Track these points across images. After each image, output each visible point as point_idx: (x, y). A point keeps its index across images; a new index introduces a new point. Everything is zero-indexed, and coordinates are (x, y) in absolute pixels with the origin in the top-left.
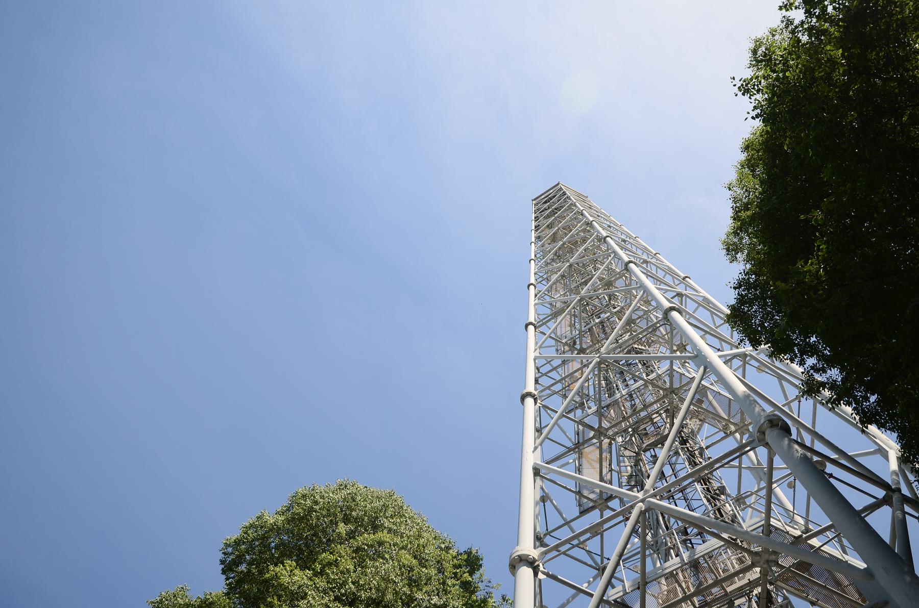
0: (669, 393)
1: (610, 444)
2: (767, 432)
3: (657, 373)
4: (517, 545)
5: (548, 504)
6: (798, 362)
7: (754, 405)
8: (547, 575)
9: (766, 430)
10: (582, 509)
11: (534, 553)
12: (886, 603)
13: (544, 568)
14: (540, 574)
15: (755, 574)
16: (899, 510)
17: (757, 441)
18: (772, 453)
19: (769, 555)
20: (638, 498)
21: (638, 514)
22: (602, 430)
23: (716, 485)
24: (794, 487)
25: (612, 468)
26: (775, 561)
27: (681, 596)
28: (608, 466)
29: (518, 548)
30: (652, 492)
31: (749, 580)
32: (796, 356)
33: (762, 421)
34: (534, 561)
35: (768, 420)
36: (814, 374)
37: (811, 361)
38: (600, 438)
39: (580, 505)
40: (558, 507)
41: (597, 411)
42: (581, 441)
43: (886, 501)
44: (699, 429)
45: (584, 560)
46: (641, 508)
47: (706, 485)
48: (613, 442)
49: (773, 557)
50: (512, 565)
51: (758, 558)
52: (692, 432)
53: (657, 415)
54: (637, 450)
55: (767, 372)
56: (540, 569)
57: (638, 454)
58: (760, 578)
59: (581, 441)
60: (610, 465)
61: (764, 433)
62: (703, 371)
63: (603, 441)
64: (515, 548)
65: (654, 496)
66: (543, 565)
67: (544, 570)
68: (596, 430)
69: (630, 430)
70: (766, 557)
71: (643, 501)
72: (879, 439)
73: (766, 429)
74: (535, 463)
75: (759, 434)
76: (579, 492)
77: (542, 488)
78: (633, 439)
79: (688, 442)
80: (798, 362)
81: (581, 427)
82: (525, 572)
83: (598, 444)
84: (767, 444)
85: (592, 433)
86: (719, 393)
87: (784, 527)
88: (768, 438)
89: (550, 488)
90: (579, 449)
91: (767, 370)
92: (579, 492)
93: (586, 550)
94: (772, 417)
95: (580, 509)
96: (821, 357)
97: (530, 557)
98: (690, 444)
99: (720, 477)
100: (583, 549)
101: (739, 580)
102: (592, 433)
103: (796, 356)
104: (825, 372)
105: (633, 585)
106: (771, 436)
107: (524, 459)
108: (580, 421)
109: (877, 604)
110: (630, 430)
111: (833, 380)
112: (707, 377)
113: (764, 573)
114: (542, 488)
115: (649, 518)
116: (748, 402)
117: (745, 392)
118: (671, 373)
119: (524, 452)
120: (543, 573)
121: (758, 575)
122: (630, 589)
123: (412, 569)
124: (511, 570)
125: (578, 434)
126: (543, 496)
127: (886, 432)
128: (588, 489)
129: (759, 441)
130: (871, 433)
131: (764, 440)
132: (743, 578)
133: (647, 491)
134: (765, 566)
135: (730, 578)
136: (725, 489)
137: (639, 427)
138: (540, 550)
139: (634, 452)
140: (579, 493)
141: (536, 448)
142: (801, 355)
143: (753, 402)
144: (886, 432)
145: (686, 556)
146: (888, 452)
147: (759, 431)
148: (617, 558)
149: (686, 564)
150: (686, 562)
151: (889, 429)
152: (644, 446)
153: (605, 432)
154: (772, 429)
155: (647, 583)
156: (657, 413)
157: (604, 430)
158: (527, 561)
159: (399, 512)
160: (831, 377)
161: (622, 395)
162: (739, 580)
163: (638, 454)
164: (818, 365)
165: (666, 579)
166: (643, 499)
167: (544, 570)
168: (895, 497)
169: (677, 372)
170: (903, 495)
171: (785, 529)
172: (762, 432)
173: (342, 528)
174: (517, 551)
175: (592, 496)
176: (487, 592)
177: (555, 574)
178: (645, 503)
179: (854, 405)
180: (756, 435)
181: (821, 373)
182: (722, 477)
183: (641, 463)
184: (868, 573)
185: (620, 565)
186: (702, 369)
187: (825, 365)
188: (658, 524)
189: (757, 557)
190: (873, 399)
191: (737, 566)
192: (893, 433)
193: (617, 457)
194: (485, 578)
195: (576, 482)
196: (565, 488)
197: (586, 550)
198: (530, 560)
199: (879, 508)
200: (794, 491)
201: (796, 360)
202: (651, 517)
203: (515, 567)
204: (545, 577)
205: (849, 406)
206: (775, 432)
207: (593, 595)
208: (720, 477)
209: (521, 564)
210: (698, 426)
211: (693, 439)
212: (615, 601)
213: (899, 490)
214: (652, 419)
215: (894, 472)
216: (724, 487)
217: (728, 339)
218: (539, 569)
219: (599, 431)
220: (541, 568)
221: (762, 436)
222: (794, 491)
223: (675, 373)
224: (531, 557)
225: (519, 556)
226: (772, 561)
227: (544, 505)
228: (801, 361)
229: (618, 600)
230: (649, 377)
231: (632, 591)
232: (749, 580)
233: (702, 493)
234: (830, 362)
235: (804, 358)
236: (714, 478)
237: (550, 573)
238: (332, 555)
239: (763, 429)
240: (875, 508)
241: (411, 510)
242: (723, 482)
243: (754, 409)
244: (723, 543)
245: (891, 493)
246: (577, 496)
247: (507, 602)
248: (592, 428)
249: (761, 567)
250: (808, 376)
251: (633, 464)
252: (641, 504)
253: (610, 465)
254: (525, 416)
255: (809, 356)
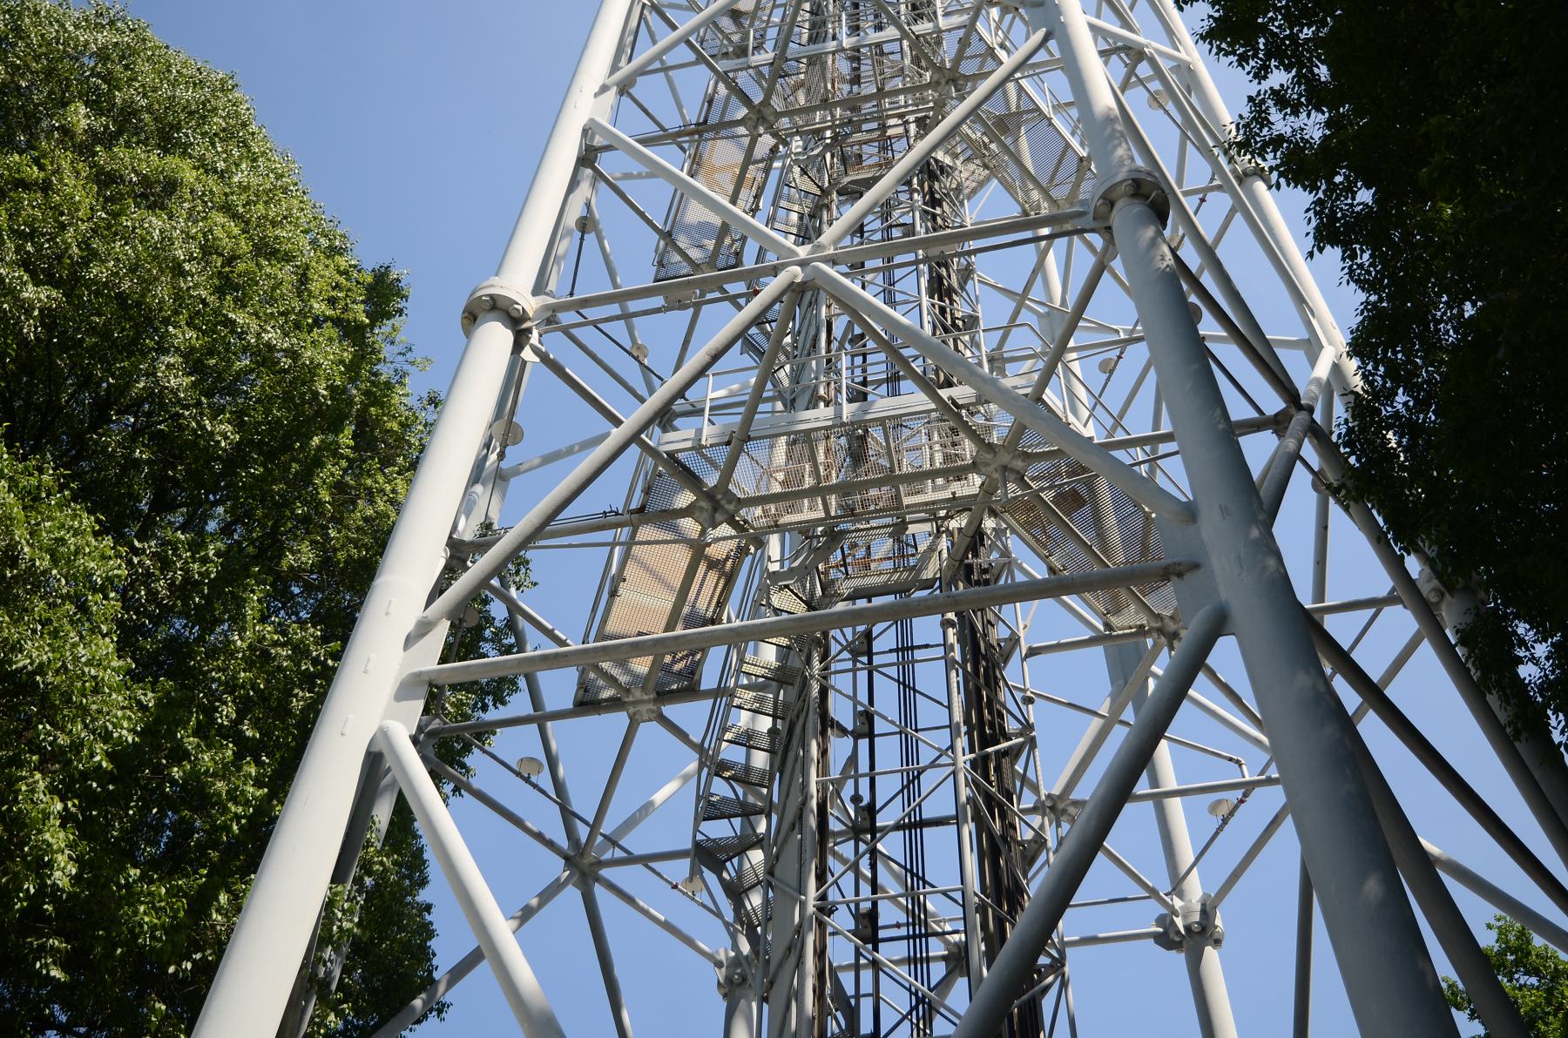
0: (943, 81)
1: (774, 150)
2: (1119, 205)
3: (937, 26)
4: (497, 275)
5: (590, 238)
6: (1253, 67)
7: (1116, 142)
8: (544, 358)
9: (1119, 198)
10: (662, 274)
11: (530, 304)
12: (1196, 566)
13: (540, 342)
14: (527, 350)
15: (973, 485)
16: (1295, 438)
17: (1091, 216)
18: (1109, 253)
19: (1014, 457)
20: (796, 254)
21: (785, 286)
22: (767, 112)
23: (961, 309)
24: (1111, 372)
25: (757, 206)
26: (1018, 472)
27: (809, 482)
28: (751, 200)
29: (494, 280)
30: (831, 251)
31: (954, 493)
32: (1255, 56)
33: (1119, 178)
34: (524, 317)
35: (1132, 180)
36: (1273, 110)
37: (1279, 78)
38: (756, 127)
39: (661, 264)
40: (612, 258)
41: (772, 64)
42: (713, 120)
43: (1277, 424)
44: (974, 191)
45: (631, 384)
46: (796, 276)
47: (941, 299)
48: (781, 147)
49: (1018, 464)
50: (470, 313)
51: (989, 456)
52: (958, 189)
53: (900, 122)
54: (826, 184)
55: (1166, 112)
56: (531, 341)
57: (825, 192)
58: (975, 496)
59: (713, 120)
60: (757, 197)
61: (1112, 204)
62: (1040, 39)
63: (760, 135)
64: (488, 279)
65: (833, 261)
66: (540, 335)
67: (540, 346)
68: (754, 107)
69: (828, 134)
70: (1005, 458)
71: (803, 264)
72: (1318, 321)
73: (1122, 196)
74: (592, 120)
75: (1101, 201)
76: (669, 234)
77: (588, 205)
78: (828, 156)
79: (941, 206)
80: (1253, 67)
81: (721, 86)
82: (495, 338)
83: (746, 141)
84: (1109, 229)
85: (742, 112)
86: (1050, 120)
87: (1065, 412)
88: (1117, 219)
89: (607, 208)
90: (700, 136)
91: (1170, 107)
92: (669, 234)
93: (641, 363)
94: (1143, 176)
95: (658, 272)
96: (1306, 78)
97: (516, 306)
98: (944, 212)
99: (977, 297)
100: (636, 358)
101: (935, 489)
102: (742, 112)
103: (1255, 56)
104: (1296, 113)
105: (723, 434)
106: (1125, 214)
107: (570, 104)
108: (726, 72)
109: (1179, 564)
110: (828, 134)
111: (1302, 139)
112: (1038, 74)
113: (988, 490)
114: (588, 205)
115: (799, 332)
116: (1109, 130)
117: (1110, 109)
118: (967, 36)
119: (575, 88)
120: (536, 351)
121: (975, 490)
122: (711, 441)
123: (231, 260)
124: (466, 322)
125: (710, 102)
126: (585, 218)
127: (1348, 283)
128: (689, 236)
129: (1094, 219)
130: (1310, 304)
131: (1106, 218)
132: (943, 488)
133: (820, 247)
134: (996, 476)
135: (919, 477)
136: (978, 323)
137: (847, 135)
138: (544, 300)
139: (818, 186)
140: (667, 236)
141: (604, 89)
142: (1269, 56)
143: (1118, 135)
144: (1348, 283)
145: (848, 410)
146: (1322, 347)
147: (1103, 197)
148: (707, 359)
149: (843, 425)
150: (845, 420)
151: (1357, 282)
152: (846, 180)
153: (771, 118)
154: (1135, 201)
155: (749, 439)
156: (901, 116)
157: (772, 114)
158: (508, 313)
159: (236, 134)
160: (1302, 129)
161: (840, 48)
162: (935, 489)
163: (825, 192)
164: (1289, 91)
165: (791, 444)
166: (804, 260)
167: (540, 346)
168: (1299, 418)
169: (981, 39)
170: (1313, 421)
171: (1066, 417)
172: (1109, 201)
173: (80, 117)
174: (492, 286)
175: (695, 254)
176: (396, 370)
177: (561, 361)
178: (808, 269)
179: (1321, 195)
180: (1095, 202)
181: (1286, 114)
182: (980, 298)
183: (825, 213)
184: (1189, 512)
185: (703, 415)
186: (1041, 33)
187: (1303, 100)
188: (814, 347)
189: (988, 453)
190: (1365, 196)
191: (938, 464)
192: (1360, 291)
193: (779, 184)
194: (401, 337)
195: (676, 190)
196: (642, 214)
197: (641, 363)
198: (514, 314)
199: (1258, 431)
200: (1108, 379)
201: (1252, 63)
202: (803, 334)
203: (475, 319)
204: (537, 360)
205: (1310, 192)
206: (1138, 208)
207: (622, 422)
208: (977, 297)
209: (491, 315)
210: (974, 184)
211: (955, 204)
212: (671, 454)
213: (1311, 410)
214: (884, 126)
215: (1317, 381)
216: (977, 318)
217: (1122, 7)
218: (529, 338)
219: (759, 111)
220: (534, 338)
221: (1105, 209)
222: (1108, 379)
223: (974, 39)
224: (519, 307)
225: (491, 296)
226: (1012, 470)
227: (582, 239)
228: (1260, 69)
229: (680, 456)
230: (914, 28)
231: (711, 446)
232: (954, 493)
233: (929, 314)
234: (1317, 96)
235: (1269, 66)
236: (964, 294)
237: (551, 356)
238: (35, 168)
239: (1113, 196)
240: (1245, 430)
241: (266, 128)
242: (979, 308)
243: (1115, 147)
244: (933, 406)
245: (1293, 410)
246: (662, 243)
247: (435, 407)
248: (746, 100)
249: (988, 476)
250: (1257, 112)
251: (807, 210)
252: (798, 269)
253: (757, 197)
254: (602, 12)
255: (1281, 63)
